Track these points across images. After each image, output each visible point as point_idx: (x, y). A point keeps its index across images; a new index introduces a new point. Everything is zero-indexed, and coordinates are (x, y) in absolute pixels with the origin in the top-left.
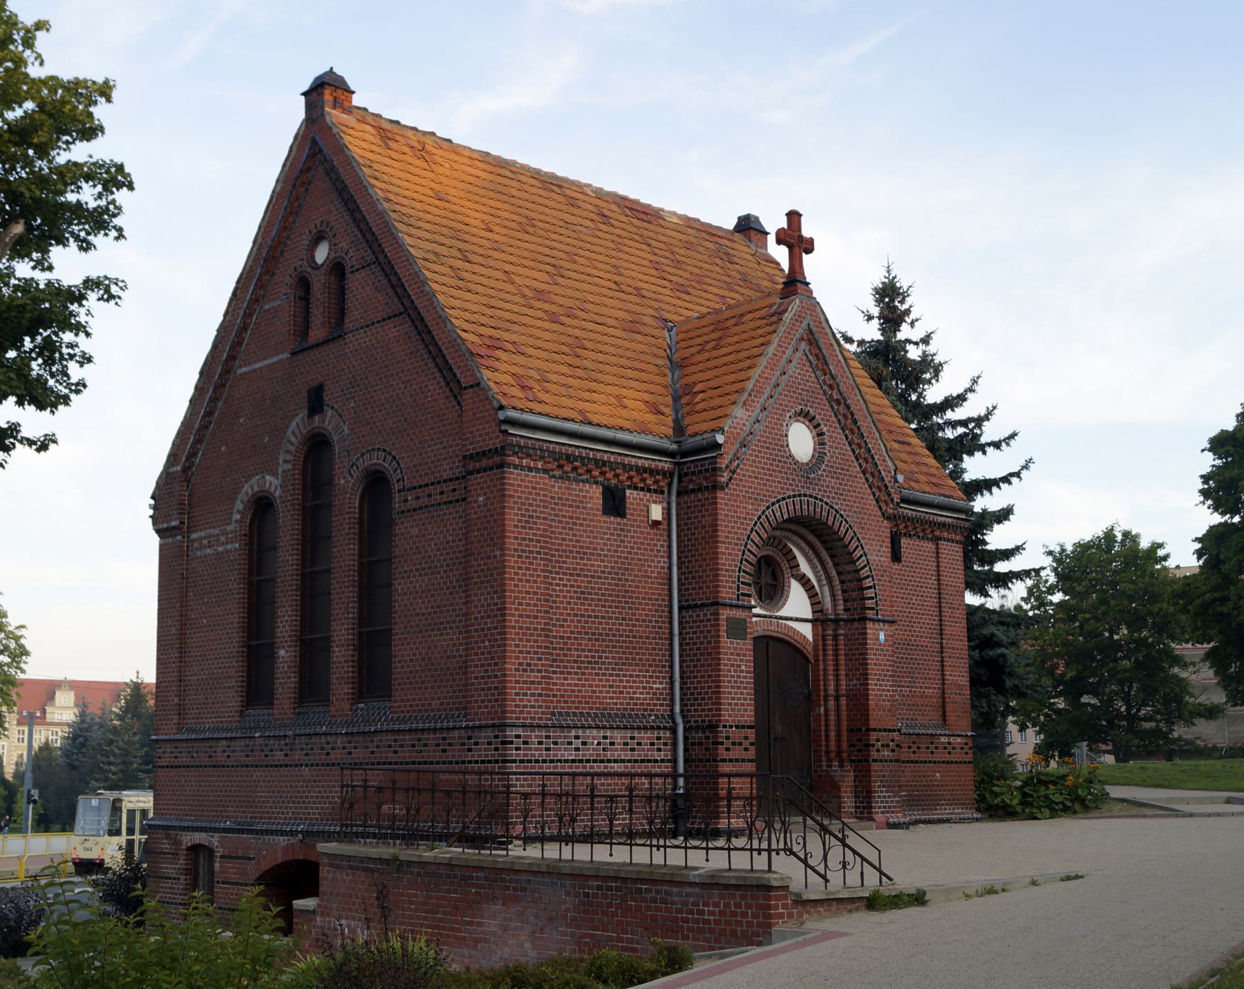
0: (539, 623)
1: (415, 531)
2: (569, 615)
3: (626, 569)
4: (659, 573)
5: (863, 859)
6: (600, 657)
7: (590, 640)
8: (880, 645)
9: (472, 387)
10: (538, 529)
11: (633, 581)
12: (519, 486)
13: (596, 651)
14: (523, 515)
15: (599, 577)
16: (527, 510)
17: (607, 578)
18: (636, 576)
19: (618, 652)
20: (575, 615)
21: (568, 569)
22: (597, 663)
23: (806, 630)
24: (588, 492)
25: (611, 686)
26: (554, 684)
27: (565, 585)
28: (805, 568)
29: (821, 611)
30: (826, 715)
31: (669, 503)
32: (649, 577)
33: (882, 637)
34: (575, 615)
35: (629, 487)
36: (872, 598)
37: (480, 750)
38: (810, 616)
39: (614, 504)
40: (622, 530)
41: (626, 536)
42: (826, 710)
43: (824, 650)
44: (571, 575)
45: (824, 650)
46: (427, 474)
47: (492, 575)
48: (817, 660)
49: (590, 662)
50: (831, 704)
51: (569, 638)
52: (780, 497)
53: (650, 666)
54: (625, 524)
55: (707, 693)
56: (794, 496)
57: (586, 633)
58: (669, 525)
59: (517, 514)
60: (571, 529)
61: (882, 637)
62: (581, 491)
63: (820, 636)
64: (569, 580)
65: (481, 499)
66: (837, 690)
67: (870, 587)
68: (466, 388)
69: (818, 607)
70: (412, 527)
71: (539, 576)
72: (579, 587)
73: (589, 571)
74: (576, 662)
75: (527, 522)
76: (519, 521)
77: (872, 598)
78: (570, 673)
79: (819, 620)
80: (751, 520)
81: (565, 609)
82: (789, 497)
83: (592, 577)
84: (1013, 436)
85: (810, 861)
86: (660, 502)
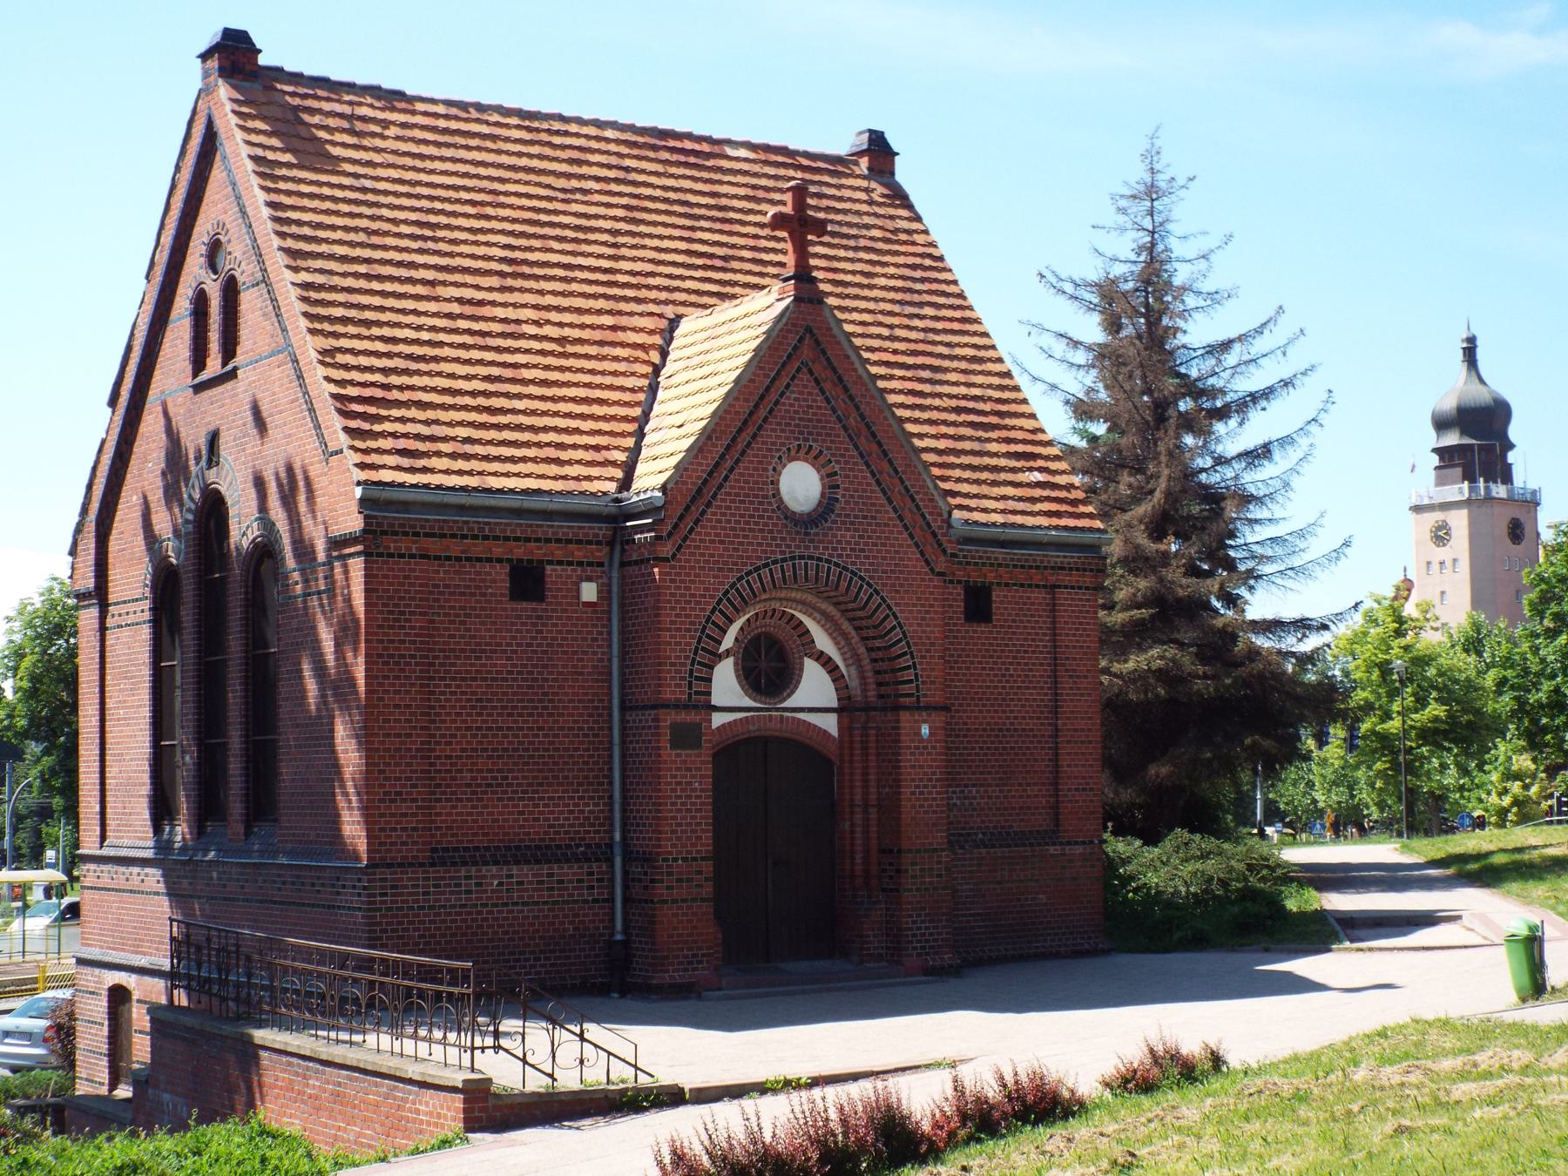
0: (415, 743)
2: (458, 729)
3: (545, 666)
4: (594, 667)
5: (610, 1054)
6: (506, 778)
7: (490, 757)
8: (922, 740)
10: (413, 628)
11: (554, 680)
12: (385, 576)
14: (390, 612)
15: (503, 679)
16: (396, 605)
17: (515, 680)
18: (560, 673)
19: (531, 771)
21: (457, 672)
23: (830, 723)
24: (489, 574)
26: (437, 814)
27: (454, 693)
28: (823, 641)
29: (849, 698)
30: (852, 832)
32: (581, 674)
33: (925, 730)
35: (550, 562)
38: (835, 704)
41: (544, 625)
44: (463, 679)
48: (842, 761)
51: (460, 757)
52: (759, 563)
53: (580, 784)
54: (546, 610)
56: (784, 560)
57: (485, 750)
59: (382, 612)
61: (925, 730)
64: (458, 686)
67: (908, 668)
71: (412, 685)
72: (473, 693)
73: (490, 672)
74: (469, 785)
75: (396, 620)
76: (385, 619)
79: (845, 708)
80: (712, 597)
81: (454, 721)
82: (775, 562)
84: (1312, 368)
85: (529, 1059)
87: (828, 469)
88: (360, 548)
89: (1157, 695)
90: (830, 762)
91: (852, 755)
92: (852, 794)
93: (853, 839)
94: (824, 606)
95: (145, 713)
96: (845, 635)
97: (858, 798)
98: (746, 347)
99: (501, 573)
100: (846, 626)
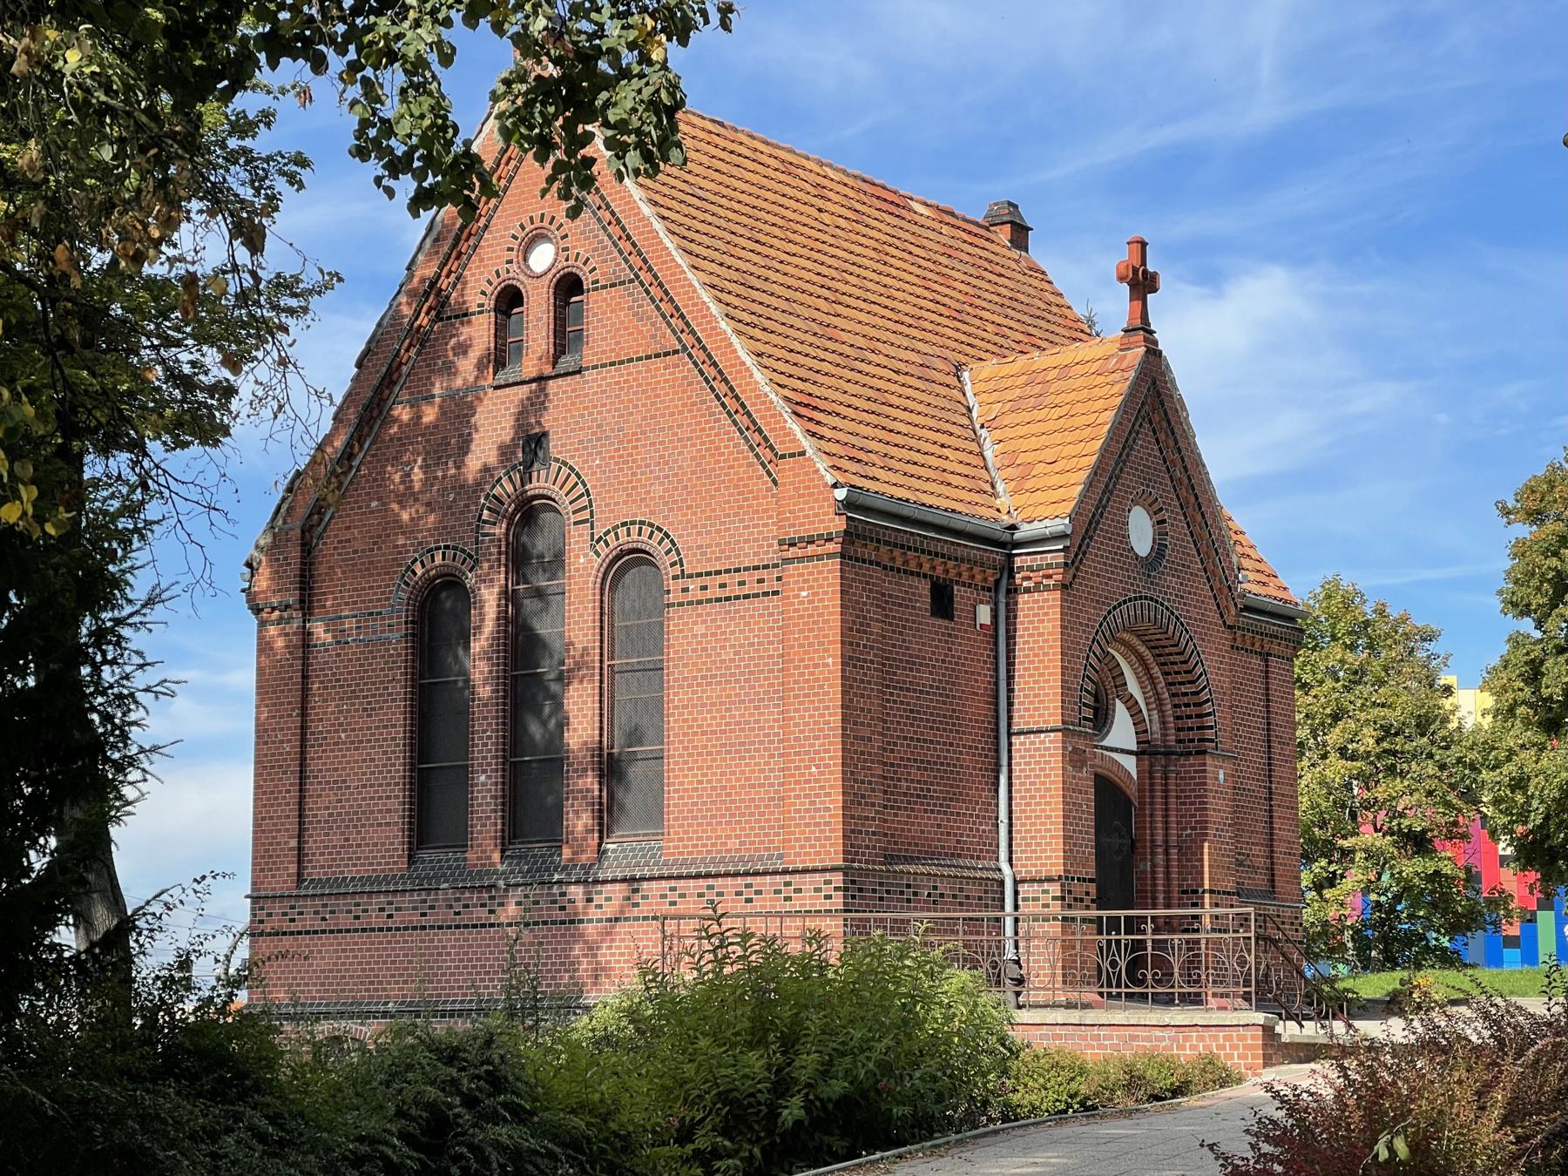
1: (700, 629)
9: (792, 455)
13: (926, 783)
15: (928, 693)
20: (905, 738)
22: (925, 797)
23: (1130, 764)
25: (939, 826)
28: (1133, 687)
30: (1154, 872)
31: (996, 604)
34: (905, 738)
35: (957, 583)
36: (1211, 727)
37: (804, 898)
38: (1134, 747)
39: (942, 602)
40: (950, 635)
42: (1154, 866)
43: (1152, 791)
44: (901, 689)
45: (1152, 791)
46: (718, 559)
47: (822, 687)
49: (918, 796)
50: (1160, 858)
55: (1044, 837)
58: (996, 630)
60: (901, 633)
62: (910, 586)
63: (1146, 773)
65: (804, 594)
66: (1166, 842)
67: (1209, 714)
68: (783, 457)
69: (1143, 737)
70: (695, 623)
77: (1211, 727)
78: (899, 808)
79: (1144, 752)
83: (921, 692)
86: (988, 603)
87: (1159, 517)
88: (832, 547)
89: (61, 1025)
90: (1129, 802)
91: (1152, 797)
92: (1152, 835)
93: (1154, 879)
94: (1142, 649)
95: (397, 767)
96: (1152, 678)
97: (1159, 839)
98: (1116, 389)
99: (924, 588)
100: (1156, 671)
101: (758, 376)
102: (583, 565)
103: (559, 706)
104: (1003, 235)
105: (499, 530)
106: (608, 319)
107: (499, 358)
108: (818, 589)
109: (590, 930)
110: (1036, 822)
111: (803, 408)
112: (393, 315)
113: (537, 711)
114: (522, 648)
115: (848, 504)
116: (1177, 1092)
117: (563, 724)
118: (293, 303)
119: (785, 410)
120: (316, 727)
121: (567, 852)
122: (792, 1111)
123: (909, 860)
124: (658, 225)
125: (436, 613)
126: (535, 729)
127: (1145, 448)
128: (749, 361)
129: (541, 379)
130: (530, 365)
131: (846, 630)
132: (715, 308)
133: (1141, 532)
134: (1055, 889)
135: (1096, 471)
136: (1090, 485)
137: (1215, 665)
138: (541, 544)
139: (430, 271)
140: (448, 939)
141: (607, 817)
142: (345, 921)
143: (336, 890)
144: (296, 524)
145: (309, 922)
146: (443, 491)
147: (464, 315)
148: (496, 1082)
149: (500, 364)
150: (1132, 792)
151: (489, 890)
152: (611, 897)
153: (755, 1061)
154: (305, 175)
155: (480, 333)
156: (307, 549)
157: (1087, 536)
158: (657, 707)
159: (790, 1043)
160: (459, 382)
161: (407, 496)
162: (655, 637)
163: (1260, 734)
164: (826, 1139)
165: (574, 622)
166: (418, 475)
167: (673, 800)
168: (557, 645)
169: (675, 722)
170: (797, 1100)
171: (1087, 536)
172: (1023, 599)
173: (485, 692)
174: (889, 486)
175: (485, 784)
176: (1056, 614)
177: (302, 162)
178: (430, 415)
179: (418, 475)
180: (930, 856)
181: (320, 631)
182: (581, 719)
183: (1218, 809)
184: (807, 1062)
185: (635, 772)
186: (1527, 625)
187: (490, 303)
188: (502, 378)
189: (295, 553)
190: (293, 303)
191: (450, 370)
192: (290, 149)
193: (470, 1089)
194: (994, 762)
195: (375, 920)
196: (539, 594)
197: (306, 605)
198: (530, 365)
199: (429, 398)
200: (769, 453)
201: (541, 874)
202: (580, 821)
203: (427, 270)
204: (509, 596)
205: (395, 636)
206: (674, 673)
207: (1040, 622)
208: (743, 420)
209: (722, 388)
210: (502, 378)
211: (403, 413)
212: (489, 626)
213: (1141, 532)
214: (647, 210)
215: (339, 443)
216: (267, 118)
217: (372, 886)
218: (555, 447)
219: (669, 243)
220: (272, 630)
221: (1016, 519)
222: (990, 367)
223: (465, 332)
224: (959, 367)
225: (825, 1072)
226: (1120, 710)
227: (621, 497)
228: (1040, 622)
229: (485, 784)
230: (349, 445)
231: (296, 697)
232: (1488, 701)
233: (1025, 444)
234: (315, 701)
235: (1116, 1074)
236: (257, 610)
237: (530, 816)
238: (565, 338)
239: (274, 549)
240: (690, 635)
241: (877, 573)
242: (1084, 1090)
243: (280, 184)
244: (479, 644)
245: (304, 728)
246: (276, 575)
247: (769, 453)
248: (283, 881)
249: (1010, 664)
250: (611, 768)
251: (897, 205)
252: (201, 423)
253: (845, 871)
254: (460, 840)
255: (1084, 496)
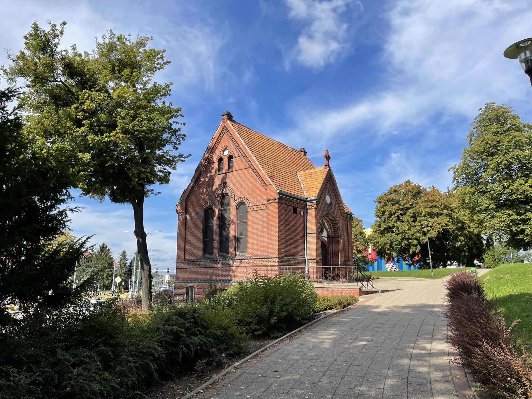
1: (253, 215)
23: (326, 239)
28: (327, 226)
39: (295, 211)
79: (328, 237)
99: (292, 208)
101: (263, 171)
102: (233, 204)
103: (228, 229)
104: (303, 153)
105: (219, 199)
106: (237, 162)
107: (219, 170)
108: (274, 208)
109: (233, 268)
110: (311, 249)
111: (271, 177)
112: (201, 163)
113: (225, 230)
114: (222, 219)
115: (279, 193)
116: (349, 305)
117: (229, 232)
118: (183, 159)
119: (268, 177)
120: (188, 233)
121: (230, 255)
122: (273, 320)
123: (290, 256)
124: (246, 146)
125: (208, 213)
126: (224, 233)
127: (329, 185)
128: (262, 169)
129: (226, 173)
130: (224, 171)
131: (279, 215)
132: (256, 160)
133: (328, 199)
134: (315, 261)
135: (321, 189)
136: (320, 191)
137: (340, 223)
138: (226, 201)
139: (207, 156)
140: (210, 269)
141: (237, 248)
142: (192, 266)
143: (190, 261)
144: (185, 198)
145: (186, 266)
146: (209, 193)
147: (213, 163)
148: (195, 323)
149: (219, 171)
150: (327, 244)
151: (217, 262)
152: (237, 263)
153: (265, 308)
154: (185, 138)
155: (216, 166)
156: (186, 203)
157: (320, 200)
158: (245, 229)
159: (273, 302)
160: (212, 174)
161: (203, 193)
162: (245, 217)
163: (346, 234)
164: (281, 325)
165: (231, 214)
166: (205, 190)
167: (248, 245)
168: (228, 219)
169: (249, 232)
170: (275, 318)
171: (320, 200)
172: (308, 210)
173: (216, 227)
174: (286, 190)
175: (216, 243)
176: (315, 213)
177: (185, 135)
178: (207, 180)
179: (205, 190)
180: (293, 255)
181: (188, 217)
182: (232, 231)
183: (341, 247)
184: (277, 308)
185: (241, 240)
186: (378, 219)
187: (217, 161)
188: (219, 173)
189: (184, 203)
190: (183, 159)
191: (210, 172)
192: (182, 134)
193: (188, 326)
194: (304, 239)
195: (197, 266)
196: (225, 210)
197: (186, 212)
198: (224, 171)
199: (207, 177)
200: (265, 185)
201: (225, 259)
202: (232, 249)
203: (207, 155)
204: (220, 210)
205: (201, 217)
206: (248, 223)
207: (312, 215)
208: (261, 179)
209: (257, 174)
210: (219, 173)
211: (202, 179)
212: (217, 216)
213: (328, 199)
214: (244, 144)
215: (192, 185)
216: (180, 129)
217: (196, 260)
218: (228, 185)
219: (248, 149)
220: (180, 217)
221: (307, 197)
222: (301, 172)
223: (213, 166)
224: (297, 172)
225: (281, 310)
226: (324, 229)
227: (239, 193)
228: (312, 215)
229: (216, 243)
230: (193, 185)
231: (184, 228)
232: (372, 230)
233: (309, 185)
234: (187, 229)
235: (337, 301)
236: (178, 213)
237: (224, 248)
238: (230, 166)
239: (180, 203)
240: (251, 216)
241: (284, 205)
242: (330, 304)
243: (181, 139)
244: (215, 219)
245: (185, 233)
246: (181, 207)
247: (265, 185)
248: (182, 259)
249: (307, 222)
250: (237, 240)
251: (285, 147)
252: (165, 179)
253: (278, 258)
254: (212, 252)
255: (319, 193)
